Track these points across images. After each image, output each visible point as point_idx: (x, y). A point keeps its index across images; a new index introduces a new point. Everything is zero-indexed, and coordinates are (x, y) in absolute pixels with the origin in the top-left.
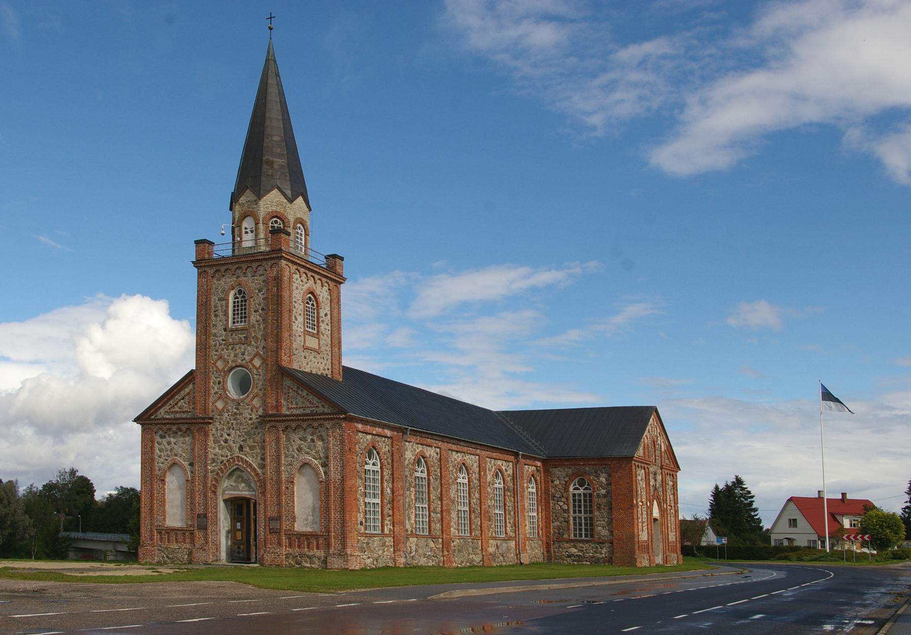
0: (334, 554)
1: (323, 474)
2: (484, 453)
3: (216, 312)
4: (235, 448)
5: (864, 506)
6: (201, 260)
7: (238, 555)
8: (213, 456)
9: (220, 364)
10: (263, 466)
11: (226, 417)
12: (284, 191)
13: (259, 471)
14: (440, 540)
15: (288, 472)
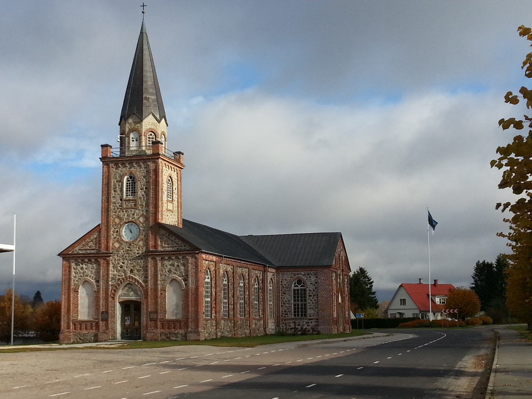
0: (191, 332)
1: (184, 285)
2: (251, 267)
3: (115, 189)
4: (127, 271)
5: (449, 289)
6: (105, 157)
7: (126, 335)
8: (113, 276)
9: (117, 221)
10: (146, 281)
11: (122, 253)
12: (156, 116)
13: (143, 284)
14: (233, 321)
15: (162, 284)
